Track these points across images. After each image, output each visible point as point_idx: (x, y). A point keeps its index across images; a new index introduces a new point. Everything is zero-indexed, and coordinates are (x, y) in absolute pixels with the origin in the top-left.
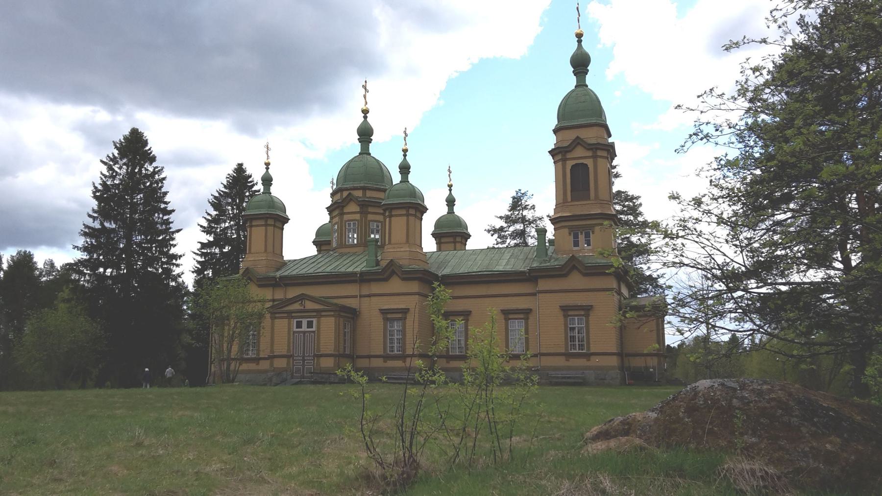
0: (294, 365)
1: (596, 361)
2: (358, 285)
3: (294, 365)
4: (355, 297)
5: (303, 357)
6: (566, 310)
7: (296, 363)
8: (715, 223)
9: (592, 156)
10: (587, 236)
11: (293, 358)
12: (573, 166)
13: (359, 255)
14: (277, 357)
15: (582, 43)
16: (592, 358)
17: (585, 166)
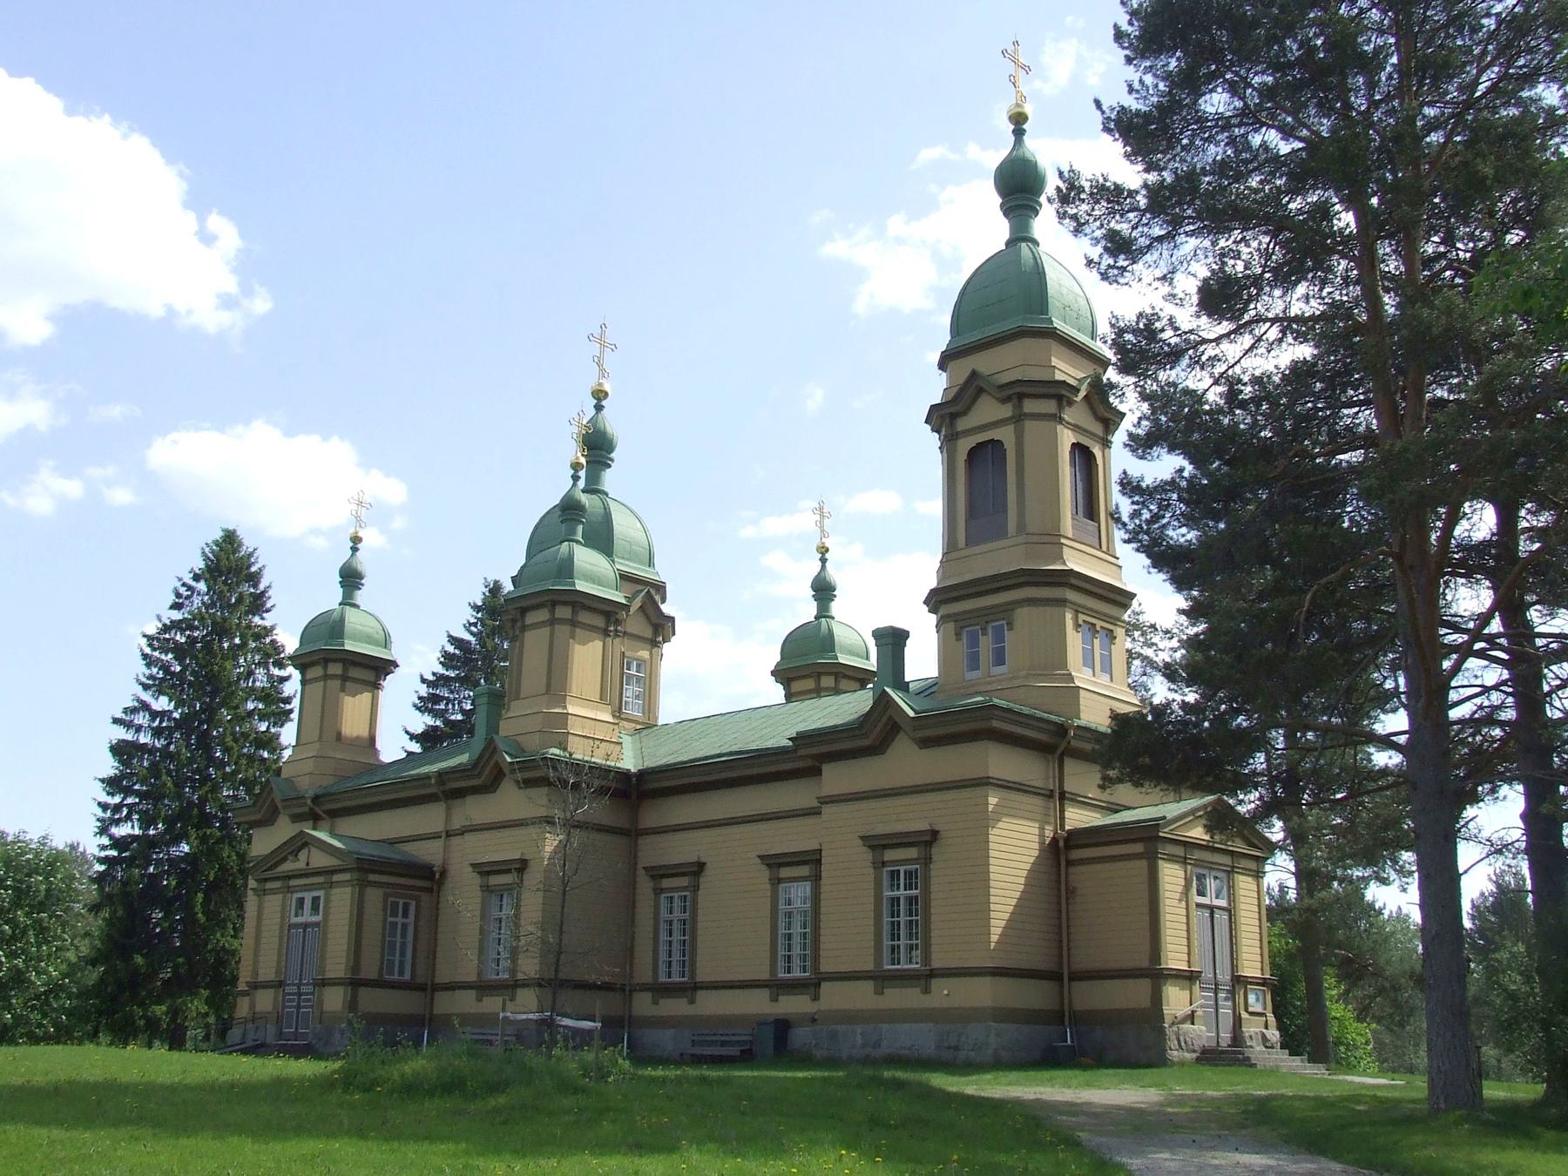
1: (945, 994)
2: (444, 805)
4: (436, 836)
9: (1012, 418)
10: (999, 638)
12: (973, 453)
13: (680, 738)
14: (707, 988)
15: (1025, 137)
16: (936, 983)
17: (996, 445)
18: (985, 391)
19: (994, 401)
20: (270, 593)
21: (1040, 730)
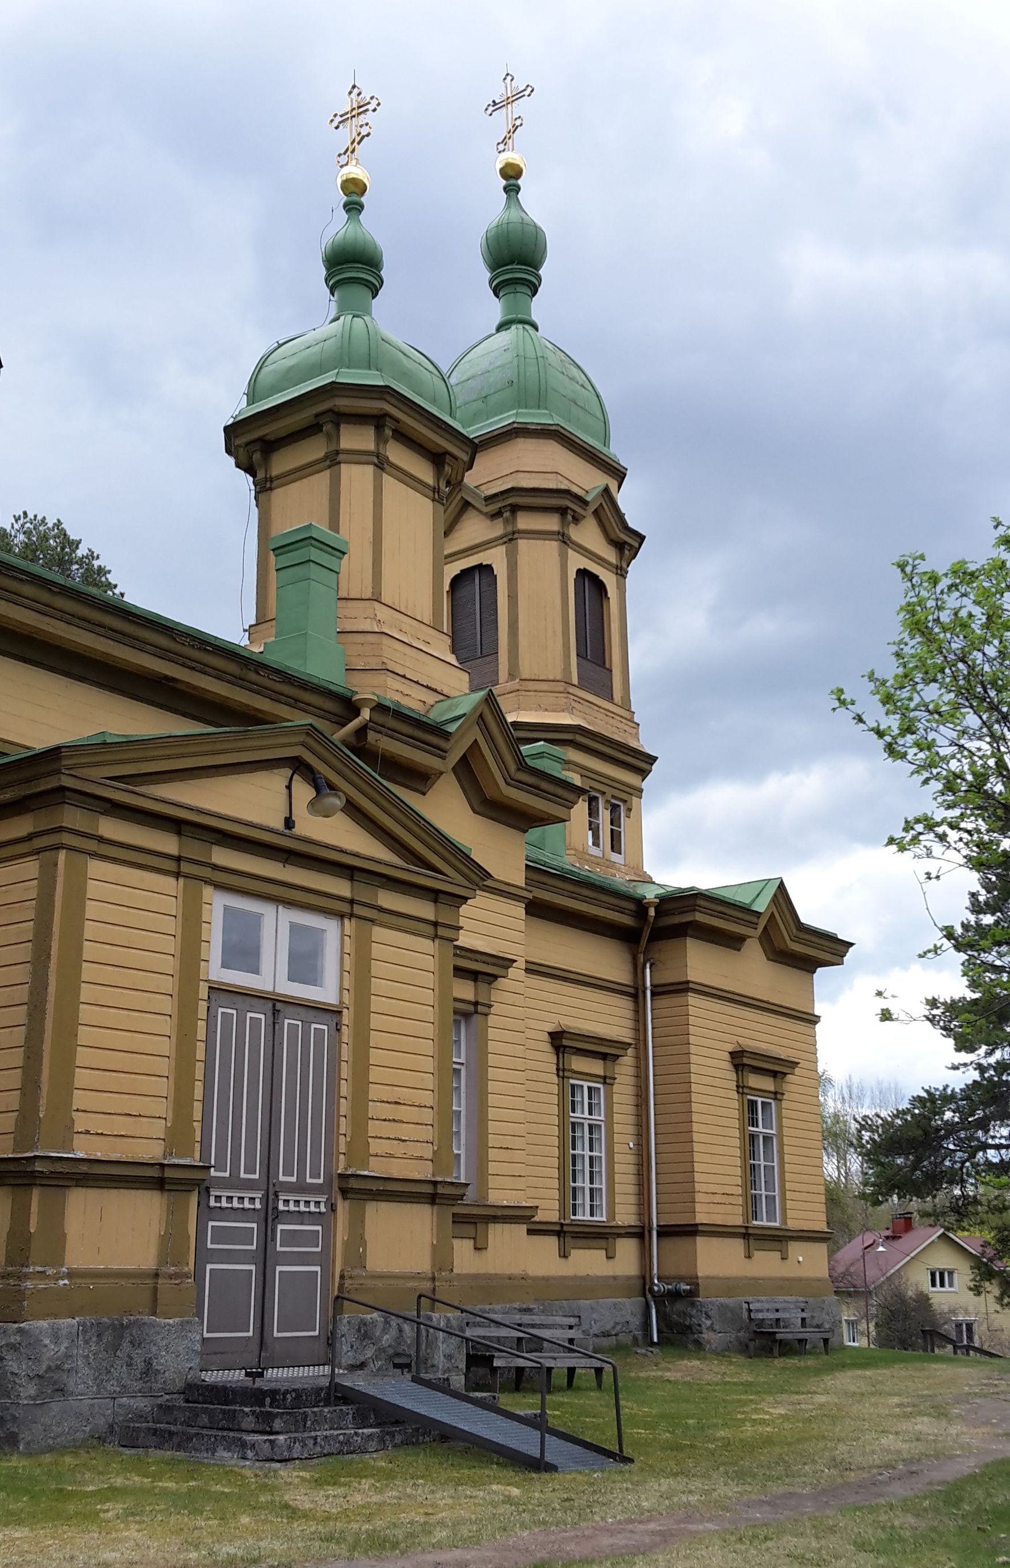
0: (203, 1256)
3: (203, 1256)
5: (271, 1195)
6: (210, 988)
7: (220, 1235)
8: (754, 900)
11: (203, 1205)
16: (498, 1234)
17: (486, 570)
18: (474, 507)
19: (482, 517)
20: (927, 1088)
21: (621, 911)
